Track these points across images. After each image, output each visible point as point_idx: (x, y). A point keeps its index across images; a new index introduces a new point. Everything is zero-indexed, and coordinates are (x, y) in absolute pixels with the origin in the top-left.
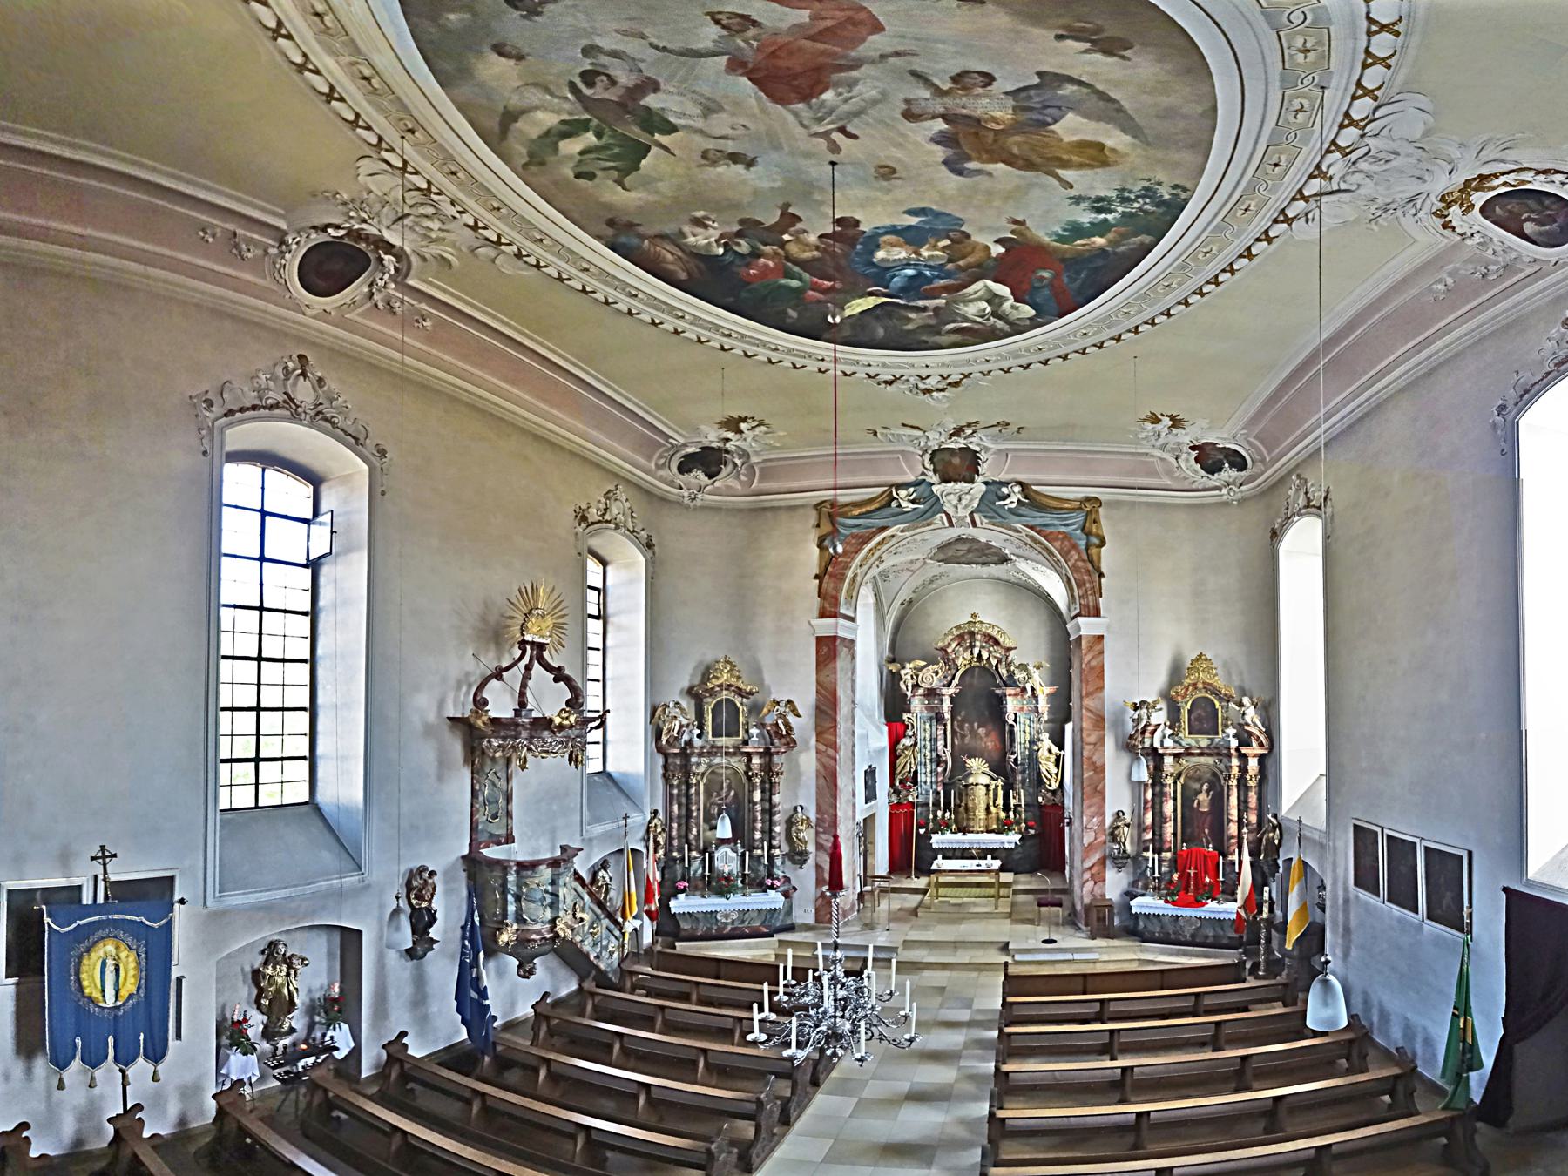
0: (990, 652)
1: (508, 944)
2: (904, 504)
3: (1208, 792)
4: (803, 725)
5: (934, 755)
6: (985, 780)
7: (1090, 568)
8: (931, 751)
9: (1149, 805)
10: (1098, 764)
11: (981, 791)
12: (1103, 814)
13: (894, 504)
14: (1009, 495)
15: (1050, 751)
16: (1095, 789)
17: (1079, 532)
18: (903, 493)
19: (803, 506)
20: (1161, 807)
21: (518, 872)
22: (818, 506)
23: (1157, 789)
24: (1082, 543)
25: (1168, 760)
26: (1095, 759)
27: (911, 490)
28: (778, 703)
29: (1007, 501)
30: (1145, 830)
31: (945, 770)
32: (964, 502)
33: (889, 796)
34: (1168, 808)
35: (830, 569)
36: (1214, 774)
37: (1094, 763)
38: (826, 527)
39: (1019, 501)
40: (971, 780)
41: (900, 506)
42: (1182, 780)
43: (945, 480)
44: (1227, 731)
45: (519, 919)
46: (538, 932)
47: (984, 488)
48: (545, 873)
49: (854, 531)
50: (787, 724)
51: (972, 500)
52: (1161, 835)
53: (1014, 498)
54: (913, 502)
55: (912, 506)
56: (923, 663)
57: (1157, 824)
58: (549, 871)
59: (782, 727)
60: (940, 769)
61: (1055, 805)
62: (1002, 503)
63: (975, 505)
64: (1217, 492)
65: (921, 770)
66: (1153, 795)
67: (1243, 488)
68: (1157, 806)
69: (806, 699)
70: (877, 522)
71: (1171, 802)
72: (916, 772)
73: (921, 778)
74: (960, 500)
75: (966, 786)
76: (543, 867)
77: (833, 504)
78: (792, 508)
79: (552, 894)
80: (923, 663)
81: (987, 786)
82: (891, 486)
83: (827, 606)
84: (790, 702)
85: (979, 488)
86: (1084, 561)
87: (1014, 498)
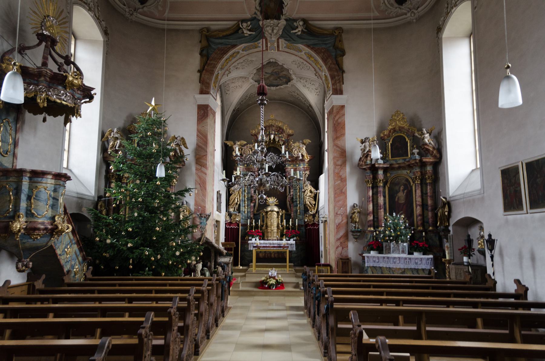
0: (279, 137)
1: (19, 231)
2: (245, 32)
3: (403, 191)
4: (189, 153)
5: (250, 196)
6: (276, 209)
7: (338, 68)
8: (248, 193)
9: (371, 199)
10: (343, 176)
11: (275, 215)
12: (346, 206)
13: (240, 32)
14: (297, 27)
15: (311, 192)
16: (342, 191)
17: (331, 48)
18: (245, 25)
19: (193, 30)
20: (377, 200)
21: (30, 178)
22: (201, 31)
23: (375, 190)
24: (334, 54)
25: (381, 172)
26: (341, 174)
27: (249, 23)
28: (176, 138)
29: (297, 31)
30: (368, 214)
31: (254, 206)
32: (275, 31)
33: (226, 217)
34: (381, 200)
35: (206, 67)
36: (407, 180)
37: (340, 176)
38: (205, 43)
39: (302, 30)
40: (269, 209)
41: (243, 33)
42: (388, 185)
43: (266, 18)
44: (414, 151)
45: (29, 214)
46: (43, 223)
47: (285, 23)
48: (49, 181)
49: (220, 46)
50: (181, 151)
51: (278, 30)
52: (378, 218)
53: (300, 29)
54: (250, 30)
55: (249, 33)
56: (245, 143)
57: (375, 211)
58: (53, 181)
59: (178, 151)
60: (252, 205)
61: (314, 224)
62: (294, 31)
63: (281, 33)
64: (404, 16)
65: (242, 204)
66: (373, 194)
67: (419, 9)
68: (375, 201)
69: (191, 141)
70: (231, 41)
71: (382, 198)
72: (240, 205)
73: (242, 209)
74: (273, 31)
75: (267, 212)
76: (50, 177)
77: (208, 29)
78: (186, 31)
79: (54, 198)
80: (245, 143)
81: (278, 212)
82: (239, 21)
83: (204, 88)
84: (183, 138)
85: (283, 22)
86: (334, 64)
87: (300, 29)
